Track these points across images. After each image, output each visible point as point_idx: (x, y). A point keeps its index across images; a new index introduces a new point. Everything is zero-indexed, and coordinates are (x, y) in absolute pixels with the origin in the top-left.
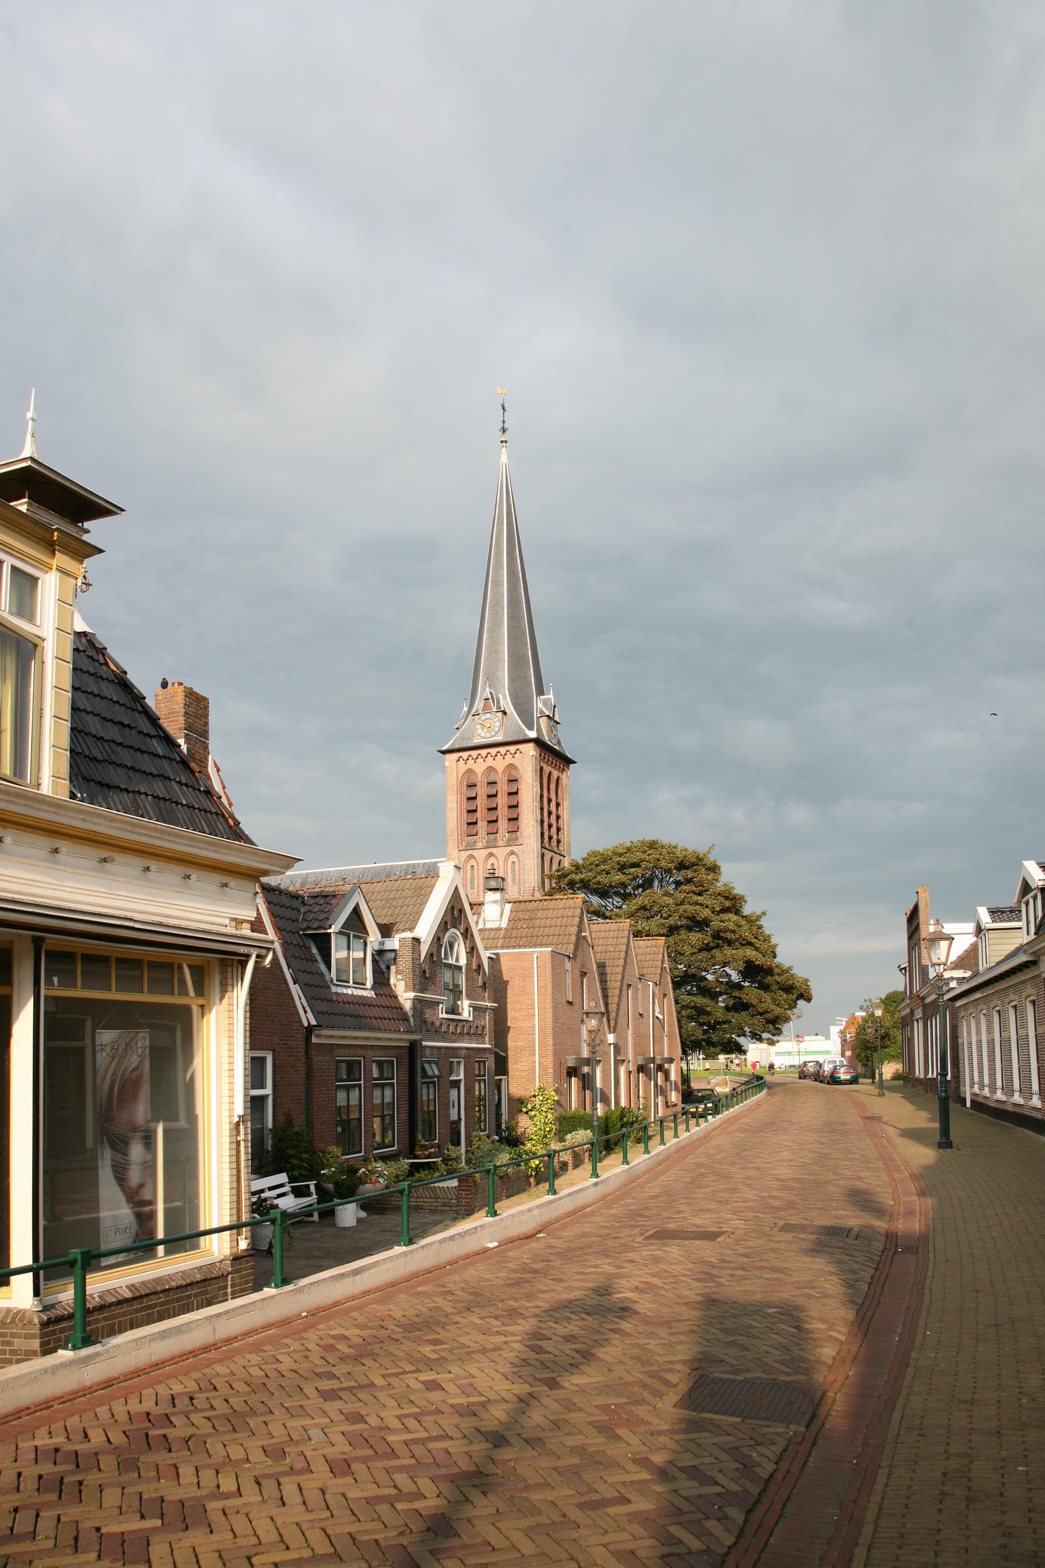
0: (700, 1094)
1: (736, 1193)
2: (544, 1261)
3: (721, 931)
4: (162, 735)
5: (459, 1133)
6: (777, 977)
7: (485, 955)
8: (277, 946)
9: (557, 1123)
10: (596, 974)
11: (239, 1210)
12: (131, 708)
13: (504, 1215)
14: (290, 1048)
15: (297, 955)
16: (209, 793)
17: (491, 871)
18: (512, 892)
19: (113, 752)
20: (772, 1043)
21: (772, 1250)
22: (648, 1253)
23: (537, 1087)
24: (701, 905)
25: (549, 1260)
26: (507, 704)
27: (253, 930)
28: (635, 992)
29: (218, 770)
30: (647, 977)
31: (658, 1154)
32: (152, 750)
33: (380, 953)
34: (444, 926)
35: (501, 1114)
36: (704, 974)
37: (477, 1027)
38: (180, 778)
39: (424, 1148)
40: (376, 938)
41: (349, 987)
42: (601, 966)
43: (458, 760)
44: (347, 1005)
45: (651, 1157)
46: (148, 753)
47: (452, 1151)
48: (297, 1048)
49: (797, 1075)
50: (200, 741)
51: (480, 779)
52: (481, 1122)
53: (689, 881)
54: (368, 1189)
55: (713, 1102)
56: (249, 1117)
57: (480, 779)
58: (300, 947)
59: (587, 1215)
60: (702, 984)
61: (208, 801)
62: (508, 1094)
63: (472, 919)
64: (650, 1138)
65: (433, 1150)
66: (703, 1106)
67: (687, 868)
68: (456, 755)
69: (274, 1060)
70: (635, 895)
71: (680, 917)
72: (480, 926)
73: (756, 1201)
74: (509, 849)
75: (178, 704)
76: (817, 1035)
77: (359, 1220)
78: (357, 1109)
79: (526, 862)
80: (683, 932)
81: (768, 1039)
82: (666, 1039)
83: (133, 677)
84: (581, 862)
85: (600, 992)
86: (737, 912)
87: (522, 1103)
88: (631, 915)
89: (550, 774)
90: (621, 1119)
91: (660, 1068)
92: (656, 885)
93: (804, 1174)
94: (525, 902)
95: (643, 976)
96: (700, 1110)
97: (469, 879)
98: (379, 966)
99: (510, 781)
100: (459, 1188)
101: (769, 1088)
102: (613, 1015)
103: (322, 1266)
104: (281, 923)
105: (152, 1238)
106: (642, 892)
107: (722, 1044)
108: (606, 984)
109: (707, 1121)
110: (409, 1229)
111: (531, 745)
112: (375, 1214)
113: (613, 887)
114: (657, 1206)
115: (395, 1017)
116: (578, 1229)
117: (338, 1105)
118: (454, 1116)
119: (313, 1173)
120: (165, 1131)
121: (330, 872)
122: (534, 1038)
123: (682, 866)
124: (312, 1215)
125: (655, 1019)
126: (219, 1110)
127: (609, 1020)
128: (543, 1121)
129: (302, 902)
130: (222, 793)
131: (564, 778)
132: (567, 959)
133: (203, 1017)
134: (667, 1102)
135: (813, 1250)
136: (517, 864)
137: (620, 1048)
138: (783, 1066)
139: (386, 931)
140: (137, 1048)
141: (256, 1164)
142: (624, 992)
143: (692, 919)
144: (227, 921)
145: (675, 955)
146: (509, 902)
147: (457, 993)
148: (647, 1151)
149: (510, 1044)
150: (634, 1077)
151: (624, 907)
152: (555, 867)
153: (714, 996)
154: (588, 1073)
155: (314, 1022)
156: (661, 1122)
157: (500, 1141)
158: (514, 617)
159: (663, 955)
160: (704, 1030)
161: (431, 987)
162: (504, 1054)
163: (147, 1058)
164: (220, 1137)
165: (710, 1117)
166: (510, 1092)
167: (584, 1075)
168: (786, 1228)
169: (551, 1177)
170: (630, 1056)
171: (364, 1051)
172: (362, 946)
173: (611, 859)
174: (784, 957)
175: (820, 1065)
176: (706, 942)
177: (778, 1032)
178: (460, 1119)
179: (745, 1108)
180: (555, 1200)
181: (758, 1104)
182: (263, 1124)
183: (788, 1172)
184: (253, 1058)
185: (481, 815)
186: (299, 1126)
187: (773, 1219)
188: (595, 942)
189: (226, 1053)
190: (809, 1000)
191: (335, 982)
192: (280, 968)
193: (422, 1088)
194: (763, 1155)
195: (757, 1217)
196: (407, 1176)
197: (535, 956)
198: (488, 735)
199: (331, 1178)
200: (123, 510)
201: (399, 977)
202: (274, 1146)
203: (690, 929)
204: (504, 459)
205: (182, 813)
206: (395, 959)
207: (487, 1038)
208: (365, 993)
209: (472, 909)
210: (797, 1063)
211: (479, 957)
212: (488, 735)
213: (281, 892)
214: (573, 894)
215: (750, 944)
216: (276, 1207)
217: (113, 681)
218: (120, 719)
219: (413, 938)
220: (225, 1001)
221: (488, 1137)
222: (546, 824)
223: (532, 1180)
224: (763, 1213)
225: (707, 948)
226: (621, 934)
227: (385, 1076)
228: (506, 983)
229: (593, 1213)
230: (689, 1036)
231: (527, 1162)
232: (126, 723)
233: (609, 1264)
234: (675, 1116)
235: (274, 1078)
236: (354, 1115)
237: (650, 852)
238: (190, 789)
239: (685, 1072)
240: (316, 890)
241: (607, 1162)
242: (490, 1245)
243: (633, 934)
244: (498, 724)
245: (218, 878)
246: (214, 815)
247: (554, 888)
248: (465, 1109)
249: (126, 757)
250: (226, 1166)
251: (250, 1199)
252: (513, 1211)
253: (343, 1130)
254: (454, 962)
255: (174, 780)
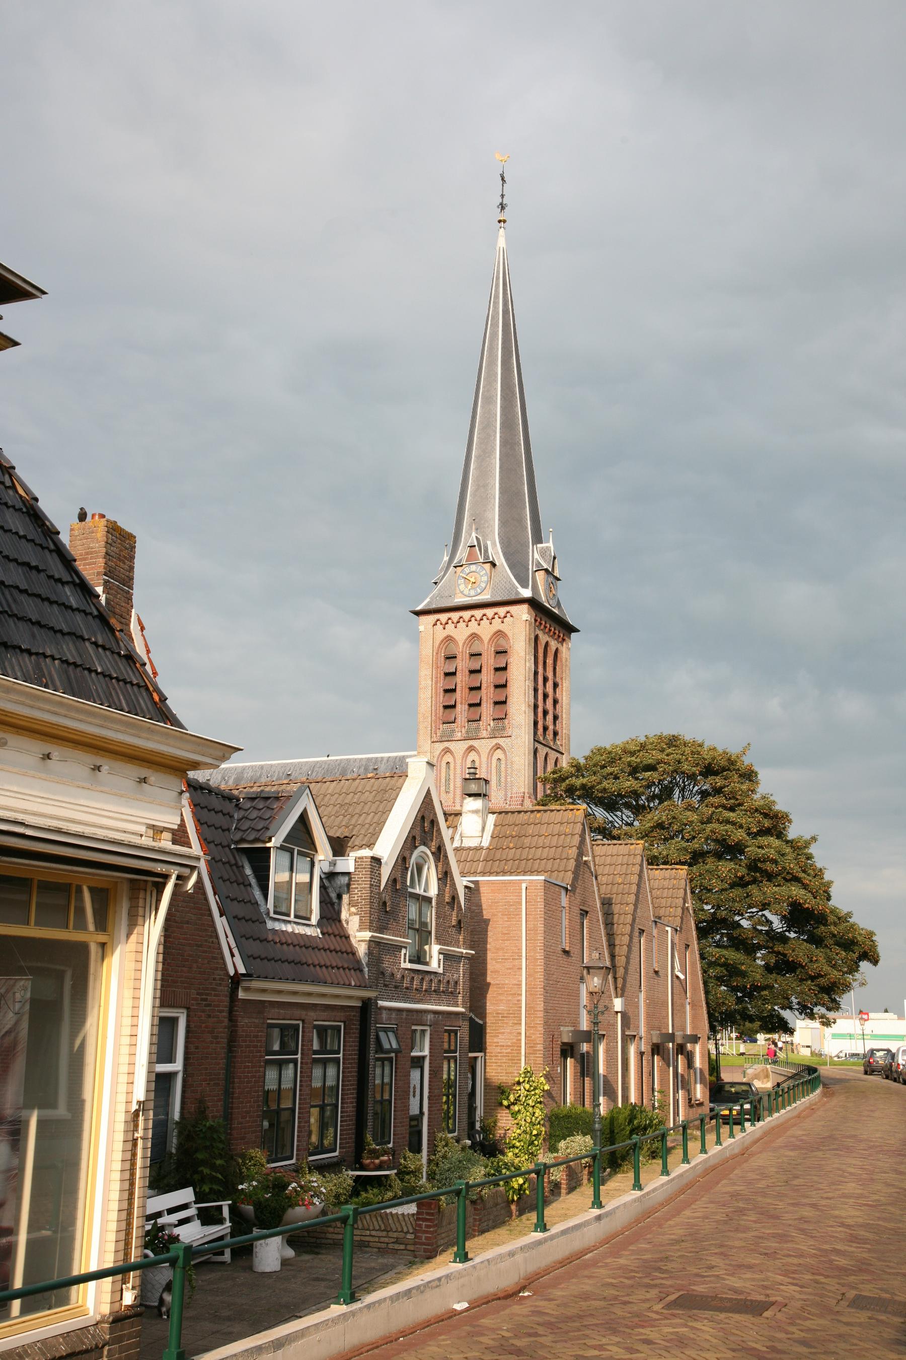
0: (733, 1090)
1: (787, 1242)
2: (530, 1335)
3: (759, 860)
4: (77, 581)
5: (420, 1133)
6: (832, 928)
7: (461, 882)
8: (202, 865)
9: (547, 1124)
10: (600, 913)
11: (127, 1244)
12: (41, 545)
13: (477, 1260)
14: (209, 1005)
15: (226, 877)
16: (130, 658)
17: (472, 771)
18: (497, 799)
19: (15, 600)
20: (827, 1023)
21: (840, 1336)
22: (671, 1330)
23: (523, 1069)
24: (733, 823)
25: (536, 1335)
26: (496, 552)
27: (174, 842)
28: (650, 941)
29: (142, 629)
30: (665, 920)
31: (681, 1176)
32: (64, 600)
33: (331, 876)
34: (411, 843)
35: (475, 1108)
36: (737, 918)
37: (448, 982)
38: (96, 638)
39: (375, 1154)
40: (326, 856)
41: (289, 922)
42: (607, 903)
43: (435, 624)
44: (285, 946)
45: (673, 1179)
46: (59, 605)
47: (410, 1161)
48: (218, 1006)
49: (862, 1068)
50: (123, 590)
51: (461, 649)
52: (449, 1118)
53: (718, 791)
54: (299, 1214)
55: (751, 1103)
56: (151, 1105)
57: (461, 649)
58: (231, 866)
59: (586, 1266)
60: (735, 933)
61: (128, 669)
62: (485, 1079)
63: (446, 833)
64: (669, 1151)
65: (385, 1158)
66: (738, 1108)
67: (716, 773)
68: (432, 618)
69: (188, 1021)
70: (651, 808)
71: (707, 839)
72: (457, 844)
73: (814, 1256)
74: (494, 741)
75: (98, 542)
76: (886, 1011)
77: (285, 1262)
78: (291, 1094)
79: (514, 759)
80: (710, 860)
81: (822, 1016)
82: (688, 1007)
83: (45, 505)
84: (582, 761)
85: (604, 939)
86: (780, 835)
87: (503, 1092)
88: (645, 835)
89: (547, 644)
90: (631, 1121)
91: (681, 1049)
92: (676, 796)
93: (879, 1219)
94: (513, 812)
95: (660, 918)
96: (734, 1113)
97: (443, 780)
98: (328, 894)
99: (498, 653)
100: (418, 1216)
101: (825, 1085)
102: (621, 972)
103: (231, 1333)
104: (210, 833)
105: (6, 1288)
106: (659, 804)
107: (761, 1019)
108: (612, 929)
109: (743, 1130)
110: (351, 1277)
111: (525, 607)
112: (306, 1252)
113: (622, 797)
114: (681, 1257)
115: (346, 966)
116: (575, 1287)
117: (266, 1088)
118: (414, 1110)
119: (228, 1190)
120: (40, 1123)
121: (271, 766)
122: (520, 1001)
123: (709, 771)
124: (222, 1253)
125: (675, 979)
126: (114, 1093)
127: (615, 979)
128: (528, 1120)
129: (237, 805)
130: (147, 661)
131: (563, 649)
132: (563, 892)
133: (103, 960)
134: (690, 1100)
135: (899, 1342)
136: (503, 762)
137: (629, 1018)
138: (842, 1055)
139: (339, 846)
140: (14, 1002)
141: (154, 1174)
142: (636, 940)
143: (721, 842)
144: (142, 829)
145: (700, 892)
146: (493, 813)
147: (424, 934)
148: (665, 1171)
149: (490, 1007)
150: (648, 1060)
151: (636, 823)
152: (550, 767)
153: (750, 950)
154: (588, 1052)
155: (242, 970)
156: (685, 1128)
157: (472, 1147)
158: (508, 443)
159: (685, 890)
160: (738, 998)
161: (392, 925)
162: (481, 1022)
163: (26, 1018)
164: (111, 1131)
165: (747, 1124)
166: (488, 1075)
167: (582, 1055)
168: (859, 1303)
169: (540, 1204)
170: (643, 1031)
171: (304, 1013)
172: (308, 867)
173: (620, 759)
174: (840, 900)
175: (893, 1056)
176: (739, 874)
177: (835, 1006)
178: (422, 1113)
179: (795, 1113)
180: (545, 1240)
181: (812, 1109)
182: (167, 1114)
183: (857, 1213)
184: (162, 1019)
185: (461, 697)
186: (214, 1117)
187: (837, 1286)
188: (600, 870)
189: (128, 1012)
190: (875, 961)
191: (272, 914)
192: (204, 893)
193: (375, 1067)
194: (820, 1186)
195: (817, 1282)
196: (351, 1196)
197: (524, 886)
198: (472, 593)
199: (251, 1197)
200: (44, 293)
201: (353, 909)
202: (180, 1147)
203: (719, 856)
204: (502, 243)
205: (95, 683)
206: (348, 885)
207: (460, 998)
208: (309, 931)
209: (446, 821)
210: (861, 1051)
211: (453, 885)
212: (472, 593)
213: (210, 791)
214: (573, 803)
215: (796, 879)
216: (175, 1239)
217: (20, 510)
218: (26, 559)
219: (372, 858)
220: (133, 938)
221: (458, 1141)
222: (540, 710)
223: (513, 1207)
224: (827, 1277)
225: (740, 883)
226: (631, 860)
227: (328, 1048)
228: (487, 922)
229: (594, 1263)
230: (718, 1005)
231: (507, 1180)
232: (33, 564)
233: (617, 1344)
234: (702, 1120)
235: (186, 1047)
236: (286, 1104)
237: (670, 750)
238: (108, 653)
239: (713, 1057)
240: (254, 789)
241: (611, 1185)
242: (459, 1307)
243: (647, 860)
244: (485, 578)
245: (135, 771)
246: (135, 688)
247: (549, 796)
248: (429, 1098)
249: (30, 607)
250: (117, 1176)
251: (143, 1226)
252: (489, 1254)
253: (271, 1125)
254: (421, 892)
255: (89, 640)
